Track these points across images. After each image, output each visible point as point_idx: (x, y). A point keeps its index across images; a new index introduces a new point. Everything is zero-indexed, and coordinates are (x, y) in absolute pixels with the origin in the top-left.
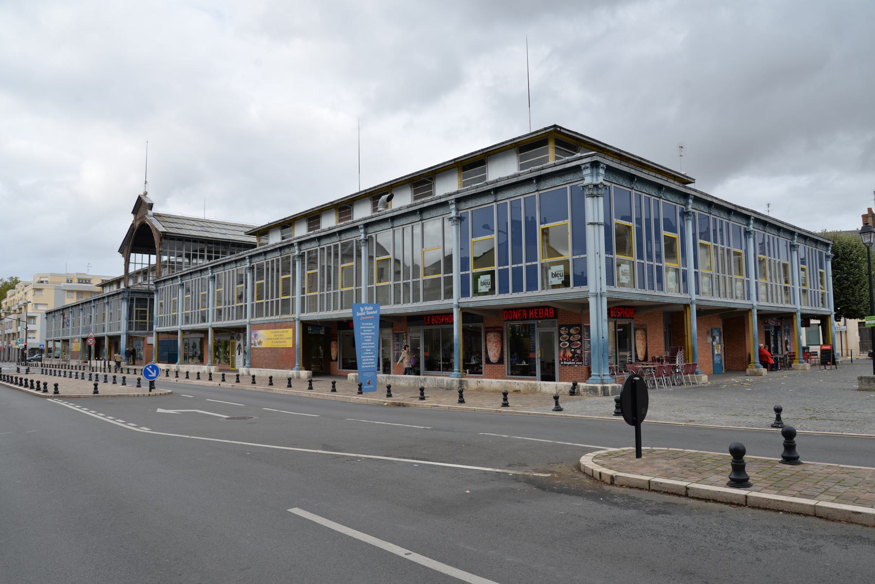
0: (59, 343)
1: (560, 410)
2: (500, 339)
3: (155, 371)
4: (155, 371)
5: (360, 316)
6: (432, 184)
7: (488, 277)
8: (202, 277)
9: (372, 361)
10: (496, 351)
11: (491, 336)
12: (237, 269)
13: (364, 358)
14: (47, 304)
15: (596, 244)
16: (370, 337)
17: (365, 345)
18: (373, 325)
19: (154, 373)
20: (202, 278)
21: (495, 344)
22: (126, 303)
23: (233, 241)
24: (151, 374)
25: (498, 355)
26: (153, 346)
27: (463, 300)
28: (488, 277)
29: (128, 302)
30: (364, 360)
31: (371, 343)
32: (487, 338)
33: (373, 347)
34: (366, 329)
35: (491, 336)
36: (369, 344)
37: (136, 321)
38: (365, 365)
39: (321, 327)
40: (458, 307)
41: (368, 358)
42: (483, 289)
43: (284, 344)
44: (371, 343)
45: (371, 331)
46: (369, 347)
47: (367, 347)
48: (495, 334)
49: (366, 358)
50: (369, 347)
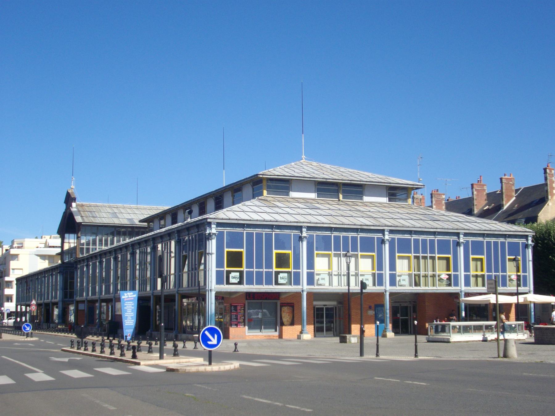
0: (335, 285)
4: (216, 336)
5: (124, 298)
6: (221, 200)
7: (238, 274)
8: (199, 233)
9: (132, 323)
10: (289, 318)
11: (285, 309)
12: (199, 234)
14: (22, 269)
16: (131, 310)
18: (133, 303)
19: (214, 337)
20: (199, 234)
21: (288, 314)
23: (136, 226)
24: (210, 340)
27: (218, 286)
31: (131, 313)
32: (282, 310)
34: (127, 305)
35: (286, 309)
36: (130, 313)
37: (70, 290)
41: (130, 322)
42: (232, 280)
44: (131, 313)
45: (131, 306)
46: (130, 315)
47: (128, 315)
48: (289, 307)
49: (127, 322)
50: (130, 315)
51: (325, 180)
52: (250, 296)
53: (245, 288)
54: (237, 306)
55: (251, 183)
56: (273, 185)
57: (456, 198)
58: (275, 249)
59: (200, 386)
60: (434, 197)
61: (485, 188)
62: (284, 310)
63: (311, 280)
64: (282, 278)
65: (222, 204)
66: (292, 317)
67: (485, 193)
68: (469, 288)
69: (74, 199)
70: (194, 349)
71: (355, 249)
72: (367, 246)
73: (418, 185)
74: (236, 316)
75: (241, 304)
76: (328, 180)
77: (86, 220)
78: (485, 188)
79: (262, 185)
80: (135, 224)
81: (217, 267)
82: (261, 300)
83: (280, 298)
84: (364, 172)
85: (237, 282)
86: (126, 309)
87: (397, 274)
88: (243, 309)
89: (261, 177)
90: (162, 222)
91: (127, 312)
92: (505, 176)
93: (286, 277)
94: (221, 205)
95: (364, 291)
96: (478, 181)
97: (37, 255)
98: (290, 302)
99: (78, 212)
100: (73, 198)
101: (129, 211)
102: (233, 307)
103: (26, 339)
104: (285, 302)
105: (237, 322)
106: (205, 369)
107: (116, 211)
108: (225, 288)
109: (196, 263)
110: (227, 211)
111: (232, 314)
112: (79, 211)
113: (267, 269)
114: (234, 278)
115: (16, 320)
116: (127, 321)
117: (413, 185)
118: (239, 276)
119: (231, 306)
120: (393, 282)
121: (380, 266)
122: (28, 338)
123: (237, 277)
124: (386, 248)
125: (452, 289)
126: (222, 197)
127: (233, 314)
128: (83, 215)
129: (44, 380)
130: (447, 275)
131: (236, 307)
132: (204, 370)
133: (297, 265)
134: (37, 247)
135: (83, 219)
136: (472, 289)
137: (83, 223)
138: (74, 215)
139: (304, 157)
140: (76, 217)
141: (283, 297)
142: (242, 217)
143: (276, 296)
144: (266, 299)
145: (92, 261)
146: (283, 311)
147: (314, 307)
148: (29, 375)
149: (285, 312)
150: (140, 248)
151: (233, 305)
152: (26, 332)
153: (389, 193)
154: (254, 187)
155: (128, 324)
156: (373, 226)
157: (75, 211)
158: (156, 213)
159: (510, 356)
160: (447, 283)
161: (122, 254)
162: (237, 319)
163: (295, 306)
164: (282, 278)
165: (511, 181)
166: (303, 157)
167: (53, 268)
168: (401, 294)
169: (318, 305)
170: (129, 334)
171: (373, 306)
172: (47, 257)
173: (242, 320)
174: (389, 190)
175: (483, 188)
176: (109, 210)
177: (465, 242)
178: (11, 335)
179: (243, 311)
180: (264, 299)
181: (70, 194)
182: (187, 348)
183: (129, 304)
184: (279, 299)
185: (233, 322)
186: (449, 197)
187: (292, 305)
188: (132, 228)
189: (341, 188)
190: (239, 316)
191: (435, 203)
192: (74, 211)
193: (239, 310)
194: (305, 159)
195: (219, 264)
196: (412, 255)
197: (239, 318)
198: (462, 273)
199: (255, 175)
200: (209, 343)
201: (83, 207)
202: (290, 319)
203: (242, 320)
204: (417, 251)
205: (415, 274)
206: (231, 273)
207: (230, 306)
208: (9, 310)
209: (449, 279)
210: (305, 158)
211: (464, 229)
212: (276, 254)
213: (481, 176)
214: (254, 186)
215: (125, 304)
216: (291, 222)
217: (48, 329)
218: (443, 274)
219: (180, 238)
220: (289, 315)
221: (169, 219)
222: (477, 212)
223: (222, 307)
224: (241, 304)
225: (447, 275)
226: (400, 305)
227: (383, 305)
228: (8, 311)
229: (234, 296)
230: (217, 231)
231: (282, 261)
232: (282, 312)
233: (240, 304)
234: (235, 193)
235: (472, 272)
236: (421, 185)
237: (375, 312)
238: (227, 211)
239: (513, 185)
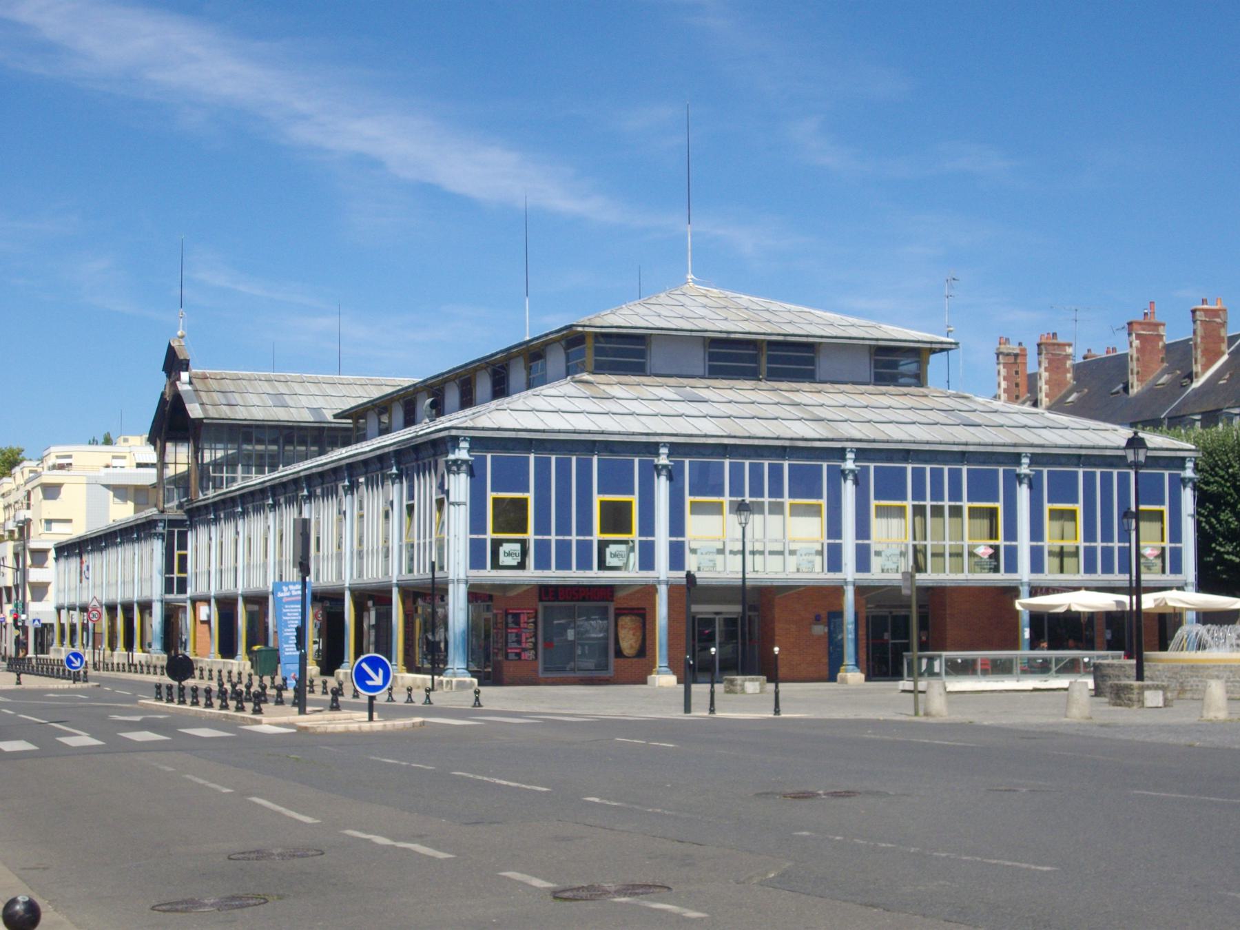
1: (412, 702)
2: (641, 625)
3: (381, 672)
4: (381, 672)
5: (282, 597)
7: (517, 547)
10: (634, 640)
11: (626, 621)
13: (287, 648)
15: (933, 445)
17: (288, 632)
19: (377, 673)
22: (160, 541)
23: (329, 425)
24: (371, 679)
25: (636, 646)
26: (941, 541)
27: (475, 573)
28: (517, 547)
29: (163, 540)
30: (287, 650)
33: (285, 630)
34: (290, 612)
35: (627, 621)
38: (289, 651)
40: (467, 582)
42: (504, 560)
45: (85, 634)
48: (634, 618)
49: (289, 648)
51: (724, 335)
52: (548, 592)
53: (532, 574)
54: (519, 614)
55: (563, 343)
56: (610, 348)
57: (1107, 352)
59: (326, 748)
60: (1046, 350)
61: (1162, 330)
62: (623, 623)
63: (677, 556)
64: (614, 555)
65: (506, 386)
66: (641, 638)
67: (1161, 344)
69: (184, 362)
70: (423, 704)
72: (805, 484)
73: (942, 343)
74: (518, 636)
75: (528, 611)
76: (732, 336)
77: (213, 413)
78: (1162, 330)
79: (584, 348)
80: (326, 421)
82: (572, 600)
83: (615, 599)
84: (825, 312)
85: (514, 563)
86: (286, 620)
87: (873, 549)
88: (532, 620)
89: (581, 332)
90: (385, 419)
91: (289, 626)
92: (1203, 304)
93: (623, 554)
94: (504, 388)
95: (918, 576)
96: (1146, 314)
97: (107, 486)
98: (636, 607)
99: (193, 392)
100: (182, 360)
101: (313, 389)
102: (510, 617)
103: (73, 686)
104: (625, 606)
105: (519, 648)
106: (360, 728)
107: (282, 388)
108: (488, 575)
109: (813, 427)
110: (534, 395)
111: (509, 631)
112: (196, 390)
113: (545, 540)
114: (509, 554)
115: (301, 652)
116: (287, 646)
117: (931, 343)
118: (520, 552)
119: (507, 614)
120: (863, 562)
122: (76, 682)
123: (515, 552)
124: (848, 490)
125: (1001, 578)
126: (506, 371)
127: (511, 633)
128: (205, 400)
129: (87, 744)
130: (991, 547)
131: (516, 617)
132: (357, 729)
133: (648, 526)
134: (107, 466)
135: (205, 410)
136: (1049, 576)
137: (205, 421)
138: (185, 401)
139: (693, 277)
140: (188, 406)
141: (620, 594)
143: (605, 592)
144: (584, 599)
145: (224, 509)
146: (622, 625)
147: (694, 618)
148: (64, 740)
149: (625, 628)
150: (322, 484)
151: (511, 611)
152: (72, 670)
153: (876, 361)
154: (569, 351)
155: (291, 653)
156: (820, 440)
157: (187, 391)
158: (353, 405)
159: (934, 712)
161: (287, 495)
162: (519, 642)
163: (647, 615)
164: (614, 555)
165: (1219, 316)
166: (690, 276)
167: (139, 522)
168: (883, 590)
169: (702, 613)
170: (292, 675)
171: (824, 614)
172: (131, 492)
173: (530, 645)
174: (876, 355)
175: (1158, 330)
176: (266, 387)
177: (1033, 473)
178: (53, 679)
179: (532, 624)
180: (578, 600)
181: (176, 350)
182: (395, 701)
183: (292, 610)
184: (612, 601)
185: (511, 648)
186: (1089, 351)
187: (642, 611)
188: (321, 429)
189: (764, 352)
190: (523, 634)
191: (1047, 365)
192: (185, 391)
193: (525, 622)
194: (694, 281)
195: (477, 523)
196: (909, 504)
197: (524, 640)
198: (1024, 543)
199: (566, 328)
200: (369, 683)
201: (206, 380)
202: (636, 642)
203: (531, 644)
204: (919, 494)
205: (915, 547)
206: (502, 546)
207: (504, 614)
208: (39, 621)
209: (995, 556)
210: (692, 279)
211: (1032, 445)
212: (603, 504)
213: (1152, 303)
214: (568, 349)
215: (284, 610)
218: (980, 545)
219: (401, 466)
220: (634, 635)
221: (398, 414)
222: (1140, 388)
223: (488, 617)
224: (529, 609)
225: (991, 547)
226: (891, 613)
227: (839, 614)
228: (37, 622)
229: (513, 593)
231: (616, 518)
232: (620, 627)
233: (525, 611)
234: (533, 361)
235: (1050, 542)
236: (951, 343)
237: (829, 629)
238: (534, 395)
239: (1224, 324)
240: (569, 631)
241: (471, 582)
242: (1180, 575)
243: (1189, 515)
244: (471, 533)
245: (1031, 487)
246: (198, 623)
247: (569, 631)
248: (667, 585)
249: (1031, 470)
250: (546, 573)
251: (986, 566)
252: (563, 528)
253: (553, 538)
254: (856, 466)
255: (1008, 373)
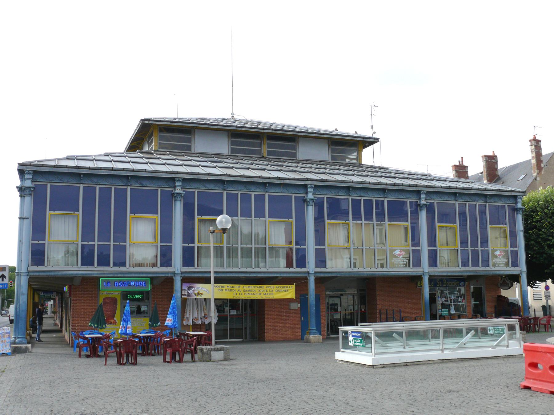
27: (35, 268)
39: (53, 292)
43: (272, 296)
58: (131, 212)
68: (435, 269)
71: (380, 216)
81: (429, 246)
121: (416, 241)
142: (307, 177)
160: (403, 262)
216: (156, 172)
217: (545, 332)
230: (314, 197)
240: (236, 311)
241: (32, 273)
242: (6, 268)
243: (520, 231)
244: (315, 246)
245: (427, 212)
246: (138, 303)
247: (236, 311)
248: (315, 276)
249: (426, 202)
250: (90, 268)
251: (401, 263)
252: (474, 244)
253: (470, 249)
254: (314, 197)
255: (540, 158)
